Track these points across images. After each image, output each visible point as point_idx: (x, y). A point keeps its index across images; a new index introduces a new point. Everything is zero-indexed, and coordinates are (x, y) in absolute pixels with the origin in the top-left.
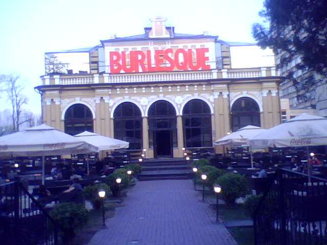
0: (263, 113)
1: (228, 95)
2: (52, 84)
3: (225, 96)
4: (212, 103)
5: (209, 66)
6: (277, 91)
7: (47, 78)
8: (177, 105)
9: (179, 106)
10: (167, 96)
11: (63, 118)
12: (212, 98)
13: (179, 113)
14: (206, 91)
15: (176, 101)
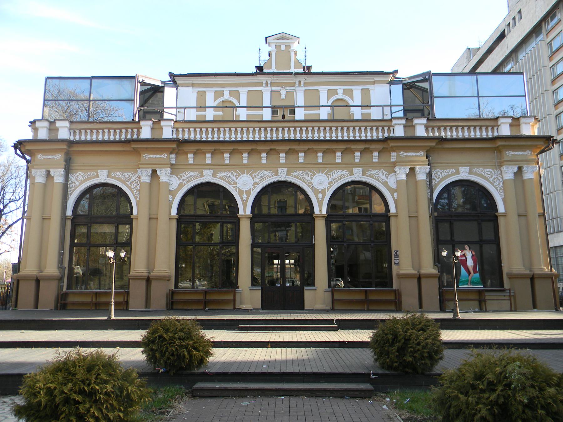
0: (504, 215)
1: (429, 174)
2: (515, 134)
3: (421, 176)
4: (392, 191)
5: (247, 111)
6: (428, 169)
7: (42, 127)
8: (241, 192)
9: (320, 195)
10: (222, 174)
11: (174, 212)
12: (392, 181)
13: (245, 211)
14: (379, 165)
15: (240, 185)
